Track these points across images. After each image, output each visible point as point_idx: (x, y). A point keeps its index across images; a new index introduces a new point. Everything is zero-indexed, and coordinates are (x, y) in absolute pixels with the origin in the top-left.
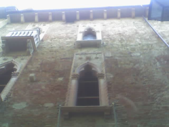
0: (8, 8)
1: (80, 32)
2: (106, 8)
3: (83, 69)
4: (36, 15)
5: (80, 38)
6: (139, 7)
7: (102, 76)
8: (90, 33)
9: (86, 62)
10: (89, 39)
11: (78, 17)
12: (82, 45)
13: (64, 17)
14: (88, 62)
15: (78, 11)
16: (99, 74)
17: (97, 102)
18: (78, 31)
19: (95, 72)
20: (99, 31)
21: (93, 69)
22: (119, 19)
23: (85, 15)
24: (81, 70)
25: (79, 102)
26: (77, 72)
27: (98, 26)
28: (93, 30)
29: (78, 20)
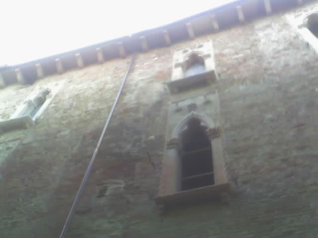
1: (177, 66)
2: (39, 61)
3: (186, 128)
5: (177, 74)
6: (127, 37)
7: (216, 133)
8: (196, 60)
9: (190, 114)
10: (193, 72)
11: (40, 72)
12: (181, 87)
13: (19, 77)
14: (193, 114)
15: (77, 53)
16: (210, 130)
17: (210, 179)
19: (205, 128)
20: (209, 56)
21: (202, 124)
23: (176, 36)
24: (183, 130)
25: (186, 184)
26: (175, 134)
29: (42, 78)
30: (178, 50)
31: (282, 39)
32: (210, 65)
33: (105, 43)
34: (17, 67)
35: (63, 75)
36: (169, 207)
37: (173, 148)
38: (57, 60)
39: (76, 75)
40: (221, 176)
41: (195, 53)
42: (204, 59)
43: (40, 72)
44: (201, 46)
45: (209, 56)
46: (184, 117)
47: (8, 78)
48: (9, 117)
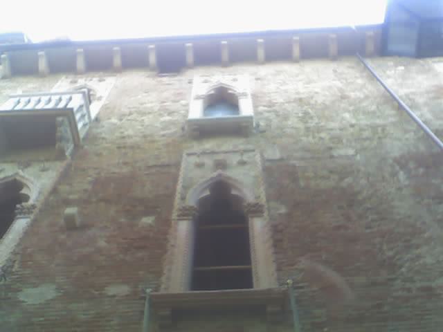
0: (357, 27)
1: (198, 98)
3: (207, 193)
4: (152, 49)
5: (196, 111)
6: (349, 29)
7: (257, 210)
8: (222, 98)
9: (215, 174)
10: (220, 114)
11: (190, 58)
12: (202, 131)
13: (152, 59)
17: (245, 278)
18: (191, 95)
19: (239, 200)
20: (244, 95)
22: (296, 61)
23: (210, 54)
25: (198, 279)
26: (191, 201)
27: (241, 80)
28: (230, 91)
31: (426, 84)
32: (246, 108)
34: (151, 41)
35: (231, 69)
37: (188, 220)
39: (136, 79)
43: (190, 58)
46: (211, 174)
47: (22, 61)
48: (187, 117)
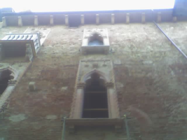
1: (86, 38)
5: (85, 43)
6: (151, 10)
7: (111, 85)
8: (96, 38)
9: (93, 70)
10: (95, 45)
11: (83, 21)
12: (87, 52)
13: (67, 21)
16: (108, 83)
17: (105, 114)
19: (103, 81)
20: (106, 37)
21: (101, 78)
23: (91, 19)
25: (85, 114)
26: (83, 80)
30: (30, 28)
33: (164, 10)
36: (75, 128)
38: (51, 16)
40: (114, 112)
41: (97, 33)
42: (104, 38)
43: (83, 21)
44: (102, 31)
45: (106, 37)
46: (91, 70)
47: (11, 20)
